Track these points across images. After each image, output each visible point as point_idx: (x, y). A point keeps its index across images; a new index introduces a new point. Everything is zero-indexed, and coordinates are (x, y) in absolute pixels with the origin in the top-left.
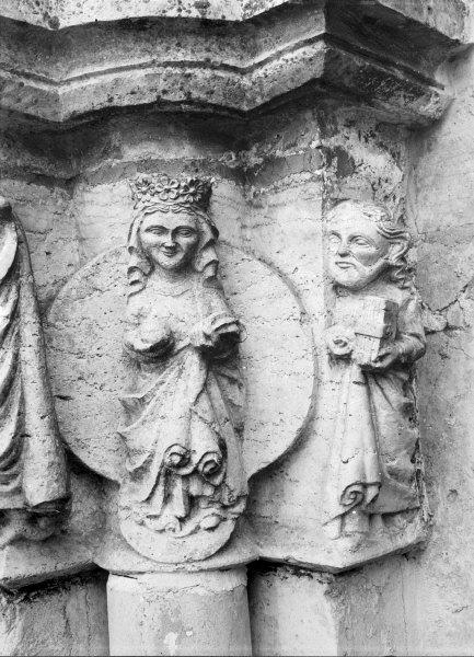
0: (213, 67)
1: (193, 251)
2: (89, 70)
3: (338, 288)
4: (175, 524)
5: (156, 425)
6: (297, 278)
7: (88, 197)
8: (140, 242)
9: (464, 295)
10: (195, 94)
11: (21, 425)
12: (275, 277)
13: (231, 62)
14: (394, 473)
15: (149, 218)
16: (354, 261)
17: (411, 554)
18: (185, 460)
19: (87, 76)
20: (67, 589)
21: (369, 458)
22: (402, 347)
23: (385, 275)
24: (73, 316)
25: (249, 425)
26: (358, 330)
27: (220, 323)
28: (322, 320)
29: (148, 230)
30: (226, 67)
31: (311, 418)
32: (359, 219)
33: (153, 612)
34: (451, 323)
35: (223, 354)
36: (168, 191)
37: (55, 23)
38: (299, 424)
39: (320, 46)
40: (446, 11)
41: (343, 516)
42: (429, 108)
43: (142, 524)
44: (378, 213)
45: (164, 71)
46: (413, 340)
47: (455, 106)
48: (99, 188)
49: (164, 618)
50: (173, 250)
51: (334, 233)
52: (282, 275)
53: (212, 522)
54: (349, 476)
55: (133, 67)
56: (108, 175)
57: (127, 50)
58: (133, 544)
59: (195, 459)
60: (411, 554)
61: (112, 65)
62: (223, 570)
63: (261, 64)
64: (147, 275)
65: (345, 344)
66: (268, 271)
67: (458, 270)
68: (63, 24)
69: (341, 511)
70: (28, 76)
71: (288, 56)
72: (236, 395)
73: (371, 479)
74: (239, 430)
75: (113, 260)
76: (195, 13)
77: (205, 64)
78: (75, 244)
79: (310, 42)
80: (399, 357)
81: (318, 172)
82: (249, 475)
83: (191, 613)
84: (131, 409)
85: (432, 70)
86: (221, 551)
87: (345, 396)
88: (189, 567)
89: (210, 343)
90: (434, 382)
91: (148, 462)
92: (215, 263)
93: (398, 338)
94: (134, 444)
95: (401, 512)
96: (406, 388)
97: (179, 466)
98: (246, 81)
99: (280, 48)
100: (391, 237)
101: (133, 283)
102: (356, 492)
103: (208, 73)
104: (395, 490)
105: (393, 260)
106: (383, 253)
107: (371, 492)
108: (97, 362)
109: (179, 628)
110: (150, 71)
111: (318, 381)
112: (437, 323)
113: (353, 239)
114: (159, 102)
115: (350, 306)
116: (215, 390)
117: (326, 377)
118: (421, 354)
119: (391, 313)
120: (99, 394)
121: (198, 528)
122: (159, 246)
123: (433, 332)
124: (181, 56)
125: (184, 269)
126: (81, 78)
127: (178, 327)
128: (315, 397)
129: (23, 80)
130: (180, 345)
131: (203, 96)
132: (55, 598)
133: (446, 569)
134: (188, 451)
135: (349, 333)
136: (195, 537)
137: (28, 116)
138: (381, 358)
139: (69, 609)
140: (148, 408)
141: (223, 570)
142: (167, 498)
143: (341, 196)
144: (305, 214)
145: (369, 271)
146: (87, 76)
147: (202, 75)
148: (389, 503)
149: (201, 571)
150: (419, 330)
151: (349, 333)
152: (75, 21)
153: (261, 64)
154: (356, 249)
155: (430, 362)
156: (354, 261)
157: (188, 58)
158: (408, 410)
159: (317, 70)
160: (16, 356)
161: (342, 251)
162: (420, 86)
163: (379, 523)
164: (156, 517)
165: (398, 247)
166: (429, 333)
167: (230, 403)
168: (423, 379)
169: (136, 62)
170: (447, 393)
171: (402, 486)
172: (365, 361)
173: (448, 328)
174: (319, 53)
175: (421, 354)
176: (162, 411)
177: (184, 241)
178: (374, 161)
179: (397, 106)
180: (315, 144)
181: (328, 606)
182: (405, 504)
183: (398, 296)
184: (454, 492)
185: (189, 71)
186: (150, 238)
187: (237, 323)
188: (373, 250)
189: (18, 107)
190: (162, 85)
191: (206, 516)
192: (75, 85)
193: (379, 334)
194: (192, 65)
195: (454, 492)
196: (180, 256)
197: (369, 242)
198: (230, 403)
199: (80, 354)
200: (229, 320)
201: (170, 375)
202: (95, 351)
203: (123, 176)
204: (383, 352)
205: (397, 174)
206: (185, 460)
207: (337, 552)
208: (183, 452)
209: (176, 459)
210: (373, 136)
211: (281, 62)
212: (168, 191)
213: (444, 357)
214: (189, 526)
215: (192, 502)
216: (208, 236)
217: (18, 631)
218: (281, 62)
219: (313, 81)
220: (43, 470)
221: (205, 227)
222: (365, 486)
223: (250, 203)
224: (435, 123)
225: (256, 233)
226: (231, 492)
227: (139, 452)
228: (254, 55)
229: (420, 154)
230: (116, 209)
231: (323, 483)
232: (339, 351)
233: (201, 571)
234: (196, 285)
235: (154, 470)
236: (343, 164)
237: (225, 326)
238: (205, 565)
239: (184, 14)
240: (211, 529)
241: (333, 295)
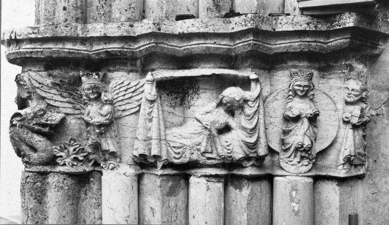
0: (317, 42)
1: (307, 91)
2: (282, 42)
3: (347, 103)
4: (296, 163)
5: (294, 137)
6: (335, 99)
7: (275, 74)
8: (293, 88)
9: (383, 106)
10: (311, 49)
11: (259, 135)
12: (329, 99)
13: (322, 41)
14: (359, 154)
15: (297, 82)
16: (352, 96)
17: (361, 177)
18: (302, 146)
19: (282, 44)
20: (262, 181)
21: (353, 149)
22: (364, 120)
23: (362, 100)
24: (270, 107)
25: (318, 138)
26: (353, 114)
27: (314, 111)
28: (342, 111)
29: (296, 85)
30: (320, 42)
31: (336, 138)
32: (355, 85)
33: (289, 186)
34: (379, 113)
35: (313, 119)
36: (303, 76)
37: (274, 30)
38: (333, 139)
39: (348, 40)
40: (384, 26)
41: (344, 164)
42: (377, 52)
43: (287, 163)
44: (361, 83)
45: (303, 43)
46: (367, 118)
47: (385, 51)
48: (280, 72)
49: (292, 187)
50: (302, 91)
51: (347, 88)
52: (331, 98)
53: (306, 163)
54: (347, 153)
55: (295, 42)
56: (282, 69)
57: (293, 37)
58: (284, 168)
59: (305, 146)
60: (361, 177)
61: (289, 41)
62: (308, 176)
63: (330, 42)
64: (294, 97)
65: (348, 118)
66: (327, 97)
67: (382, 98)
68: (277, 30)
69: (344, 162)
70: (265, 43)
71: (339, 41)
72: (316, 130)
73: (352, 154)
74: (315, 140)
75: (282, 92)
76: (314, 29)
77: (315, 41)
78: (269, 86)
79: (347, 38)
80: (364, 122)
81: (344, 71)
82: (317, 152)
83: (300, 187)
84: (285, 133)
85: (378, 41)
86: (308, 172)
87: (348, 131)
88: (300, 175)
89: (311, 116)
90: (372, 130)
91: (290, 147)
92: (313, 95)
93: (363, 117)
94: (287, 141)
95: (359, 165)
96: (364, 131)
97: (300, 148)
98: (325, 46)
99: (337, 39)
100: (364, 90)
101: (290, 99)
102: (348, 158)
103: (315, 44)
104: (359, 158)
105: (364, 96)
106: (361, 94)
107: (353, 158)
108: (275, 120)
109: (296, 190)
110: (300, 43)
111: (339, 127)
112: (374, 113)
113: (353, 90)
114: (301, 51)
115: (351, 108)
116: (311, 128)
117: (341, 127)
118: (369, 121)
119: (362, 110)
120: (275, 128)
121: (303, 165)
122: (299, 90)
123: (373, 115)
124: (308, 39)
125: (305, 96)
126: (280, 44)
127: (302, 111)
128: (286, 171)
129: (264, 45)
130: (303, 116)
131: (313, 50)
132: (259, 182)
133: (371, 182)
134: (303, 144)
135: (350, 115)
136: (302, 167)
137: (264, 53)
138: (358, 122)
139: (262, 186)
140: (292, 132)
141: (308, 176)
142: (295, 156)
143: (349, 77)
144: (338, 82)
145: (356, 99)
146: (282, 44)
147: (313, 44)
148: (357, 162)
149: (303, 176)
150: (369, 115)
151: (350, 115)
152: (280, 30)
153: (330, 42)
154: (353, 93)
155: (371, 124)
156: (352, 96)
157: (310, 40)
158: (364, 137)
159: (347, 45)
160: (258, 117)
161: (349, 93)
162: (375, 46)
163: (353, 167)
164: (291, 161)
165: (365, 93)
166: (372, 116)
167: (314, 132)
168: (368, 129)
169: (296, 41)
170: (375, 133)
171: (361, 157)
172: (354, 123)
173: (377, 115)
174: (349, 42)
175: (369, 121)
176: (296, 133)
177: (306, 89)
178: (359, 67)
179: (369, 52)
180: (343, 63)
181: (337, 188)
182: (361, 163)
183: (364, 106)
184: (375, 161)
185: (310, 43)
186: (297, 88)
187: (318, 111)
188: (358, 93)
189: (262, 51)
190: (303, 47)
191: (305, 162)
192: (278, 46)
193: (359, 116)
194: (311, 42)
195: (375, 161)
196: (304, 93)
197: (357, 91)
198: (314, 132)
199: (271, 117)
200: (317, 110)
201: (299, 124)
202: (275, 116)
203: (287, 69)
204: (359, 121)
205: (365, 70)
206: (302, 146)
207: (342, 173)
208: (302, 144)
209: (300, 146)
210: (359, 59)
211: (336, 42)
212: (303, 76)
213: (376, 123)
214: (300, 164)
215: (302, 158)
216: (312, 88)
217: (250, 189)
218: (336, 42)
219: (345, 48)
220: (263, 147)
221: (312, 85)
222: (351, 156)
223: (321, 77)
224: (378, 55)
225: (322, 85)
226: (312, 156)
227: (288, 144)
228: (328, 39)
229: (373, 63)
230: (284, 78)
231: (338, 155)
232: (346, 120)
233: (303, 176)
234: (307, 100)
235: (292, 149)
236: (351, 68)
237: (316, 112)
238: (304, 175)
239: (311, 29)
240: (306, 165)
241: (345, 104)
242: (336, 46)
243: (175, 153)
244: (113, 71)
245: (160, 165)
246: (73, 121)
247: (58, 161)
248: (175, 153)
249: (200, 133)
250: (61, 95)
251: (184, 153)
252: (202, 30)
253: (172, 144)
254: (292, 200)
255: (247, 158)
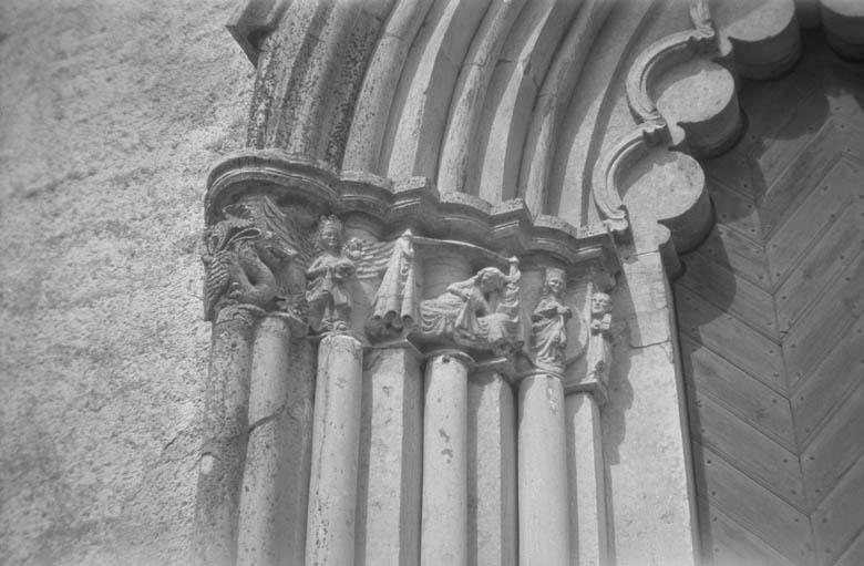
50: (557, 288)
142: (550, 355)
242: (586, 255)
243: (425, 322)
244: (354, 228)
245: (406, 332)
246: (296, 271)
247: (279, 303)
248: (425, 322)
249: (455, 306)
250: (290, 235)
251: (436, 324)
252: (617, 513)
253: (423, 312)
254: (549, 397)
255: (502, 344)
